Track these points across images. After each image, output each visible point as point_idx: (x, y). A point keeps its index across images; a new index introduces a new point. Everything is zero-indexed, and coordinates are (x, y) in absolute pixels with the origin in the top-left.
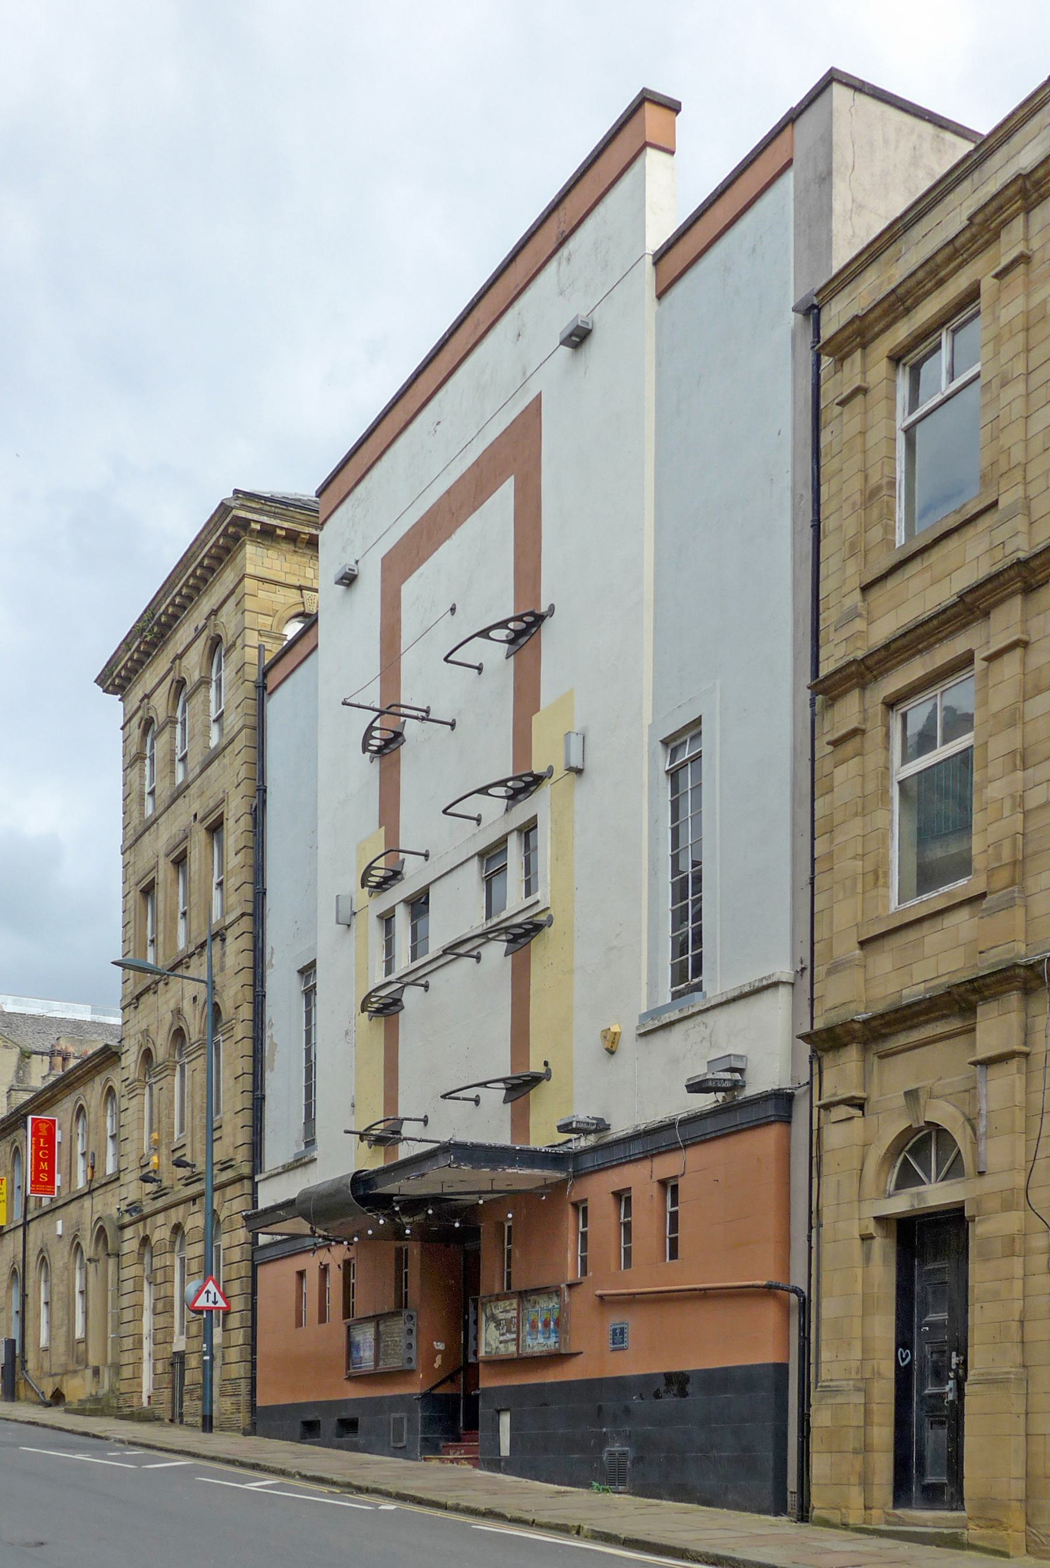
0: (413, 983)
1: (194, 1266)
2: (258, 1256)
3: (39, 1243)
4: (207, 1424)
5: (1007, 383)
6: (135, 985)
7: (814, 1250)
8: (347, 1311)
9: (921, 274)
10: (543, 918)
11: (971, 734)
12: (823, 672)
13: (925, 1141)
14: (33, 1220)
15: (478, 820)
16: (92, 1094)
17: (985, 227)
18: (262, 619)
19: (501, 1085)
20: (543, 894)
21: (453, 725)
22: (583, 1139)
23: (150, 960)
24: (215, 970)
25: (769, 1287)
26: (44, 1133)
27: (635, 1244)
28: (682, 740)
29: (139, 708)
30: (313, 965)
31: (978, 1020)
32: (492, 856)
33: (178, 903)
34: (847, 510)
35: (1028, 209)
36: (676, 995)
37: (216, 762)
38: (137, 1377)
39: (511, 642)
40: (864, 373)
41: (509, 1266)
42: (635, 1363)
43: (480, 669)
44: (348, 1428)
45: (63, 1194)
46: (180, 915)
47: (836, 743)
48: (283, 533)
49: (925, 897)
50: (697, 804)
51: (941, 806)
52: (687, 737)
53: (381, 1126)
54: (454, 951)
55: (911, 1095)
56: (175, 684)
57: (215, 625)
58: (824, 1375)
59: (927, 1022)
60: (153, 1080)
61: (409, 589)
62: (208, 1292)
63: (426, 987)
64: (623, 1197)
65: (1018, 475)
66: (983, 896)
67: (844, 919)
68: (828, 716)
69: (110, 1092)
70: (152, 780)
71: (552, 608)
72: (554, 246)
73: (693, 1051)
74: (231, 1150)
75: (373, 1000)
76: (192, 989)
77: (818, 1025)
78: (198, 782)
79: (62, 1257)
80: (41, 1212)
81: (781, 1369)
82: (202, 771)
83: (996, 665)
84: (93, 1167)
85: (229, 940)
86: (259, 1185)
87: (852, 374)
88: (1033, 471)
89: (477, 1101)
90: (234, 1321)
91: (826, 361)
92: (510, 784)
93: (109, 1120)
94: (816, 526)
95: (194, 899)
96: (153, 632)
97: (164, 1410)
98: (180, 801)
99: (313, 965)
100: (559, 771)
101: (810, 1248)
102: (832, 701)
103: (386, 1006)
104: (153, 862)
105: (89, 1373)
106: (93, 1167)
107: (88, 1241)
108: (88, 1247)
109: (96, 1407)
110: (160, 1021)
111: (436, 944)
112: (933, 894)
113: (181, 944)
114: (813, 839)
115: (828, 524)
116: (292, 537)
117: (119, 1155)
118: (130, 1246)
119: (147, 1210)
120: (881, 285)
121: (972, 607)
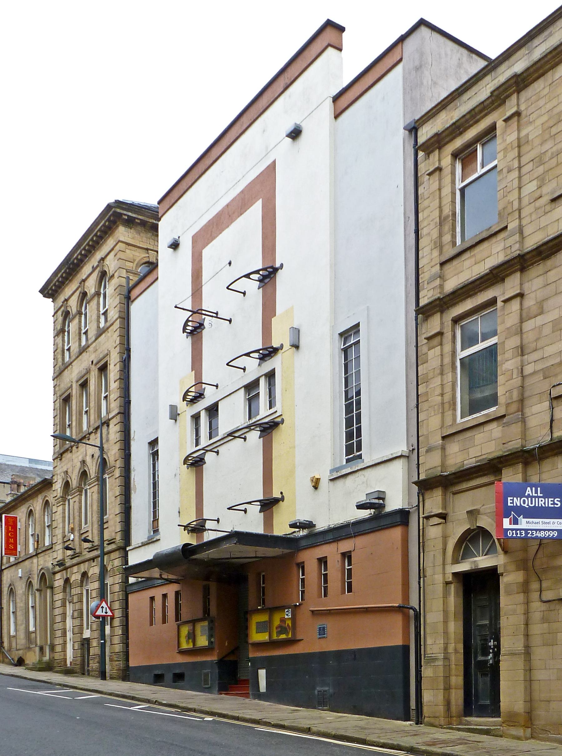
0: (211, 451)
1: (94, 594)
2: (129, 589)
3: (9, 580)
4: (103, 676)
5: (511, 171)
6: (60, 448)
7: (422, 589)
8: (178, 617)
9: (468, 116)
10: (279, 420)
11: (496, 337)
12: (421, 304)
13: (478, 534)
14: (5, 569)
15: (244, 369)
16: (37, 504)
17: (498, 98)
18: (128, 264)
19: (259, 503)
20: (278, 407)
21: (230, 321)
22: (301, 531)
23: (68, 434)
24: (104, 441)
25: (399, 607)
26: (11, 523)
27: (329, 585)
28: (350, 333)
29: (62, 306)
30: (356, 328)
31: (503, 477)
32: (251, 387)
33: (83, 406)
34: (432, 225)
35: (519, 92)
36: (348, 461)
37: (104, 335)
38: (64, 650)
39: (260, 281)
40: (439, 160)
41: (264, 595)
42: (330, 645)
43: (244, 293)
44: (178, 678)
45: (22, 555)
46: (84, 412)
47: (429, 339)
48: (139, 221)
49: (474, 416)
50: (358, 365)
51: (480, 372)
52: (352, 332)
53: (195, 523)
54: (232, 435)
55: (470, 513)
56: (81, 294)
57: (103, 266)
58: (429, 651)
59: (477, 477)
60: (70, 497)
61: (207, 252)
62: (102, 607)
63: (217, 453)
64: (323, 561)
65: (516, 214)
66: (504, 416)
67: (433, 424)
68: (424, 326)
69: (47, 504)
70: (69, 343)
71: (282, 265)
72: (282, 90)
73: (360, 488)
74: (114, 534)
75: (190, 458)
76: (91, 450)
77: (422, 477)
78: (94, 344)
79: (22, 588)
80: (10, 565)
81: (406, 649)
82: (96, 339)
83: (508, 305)
84: (38, 542)
85: (111, 426)
86: (129, 553)
87: (433, 161)
88: (524, 213)
89: (245, 511)
90: (117, 622)
91: (421, 154)
92: (261, 352)
93: (46, 517)
94: (417, 232)
95: (92, 404)
96: (70, 267)
97: (77, 668)
98: (84, 354)
99: (356, 328)
100: (287, 346)
101: (420, 588)
102: (426, 318)
103: (196, 462)
104: (69, 385)
105: (37, 649)
106: (38, 542)
107: (36, 581)
108: (36, 582)
109: (48, 667)
110: (74, 467)
111: (223, 430)
112: (478, 415)
113: (85, 428)
114: (418, 385)
115: (423, 232)
116: (143, 224)
117: (52, 536)
118: (59, 582)
119: (68, 564)
120: (447, 120)
121: (496, 276)
